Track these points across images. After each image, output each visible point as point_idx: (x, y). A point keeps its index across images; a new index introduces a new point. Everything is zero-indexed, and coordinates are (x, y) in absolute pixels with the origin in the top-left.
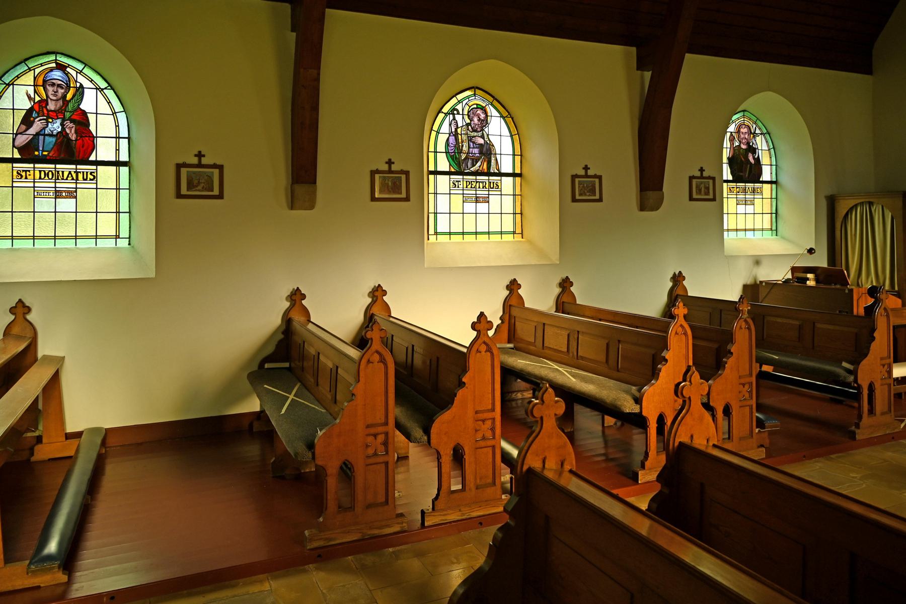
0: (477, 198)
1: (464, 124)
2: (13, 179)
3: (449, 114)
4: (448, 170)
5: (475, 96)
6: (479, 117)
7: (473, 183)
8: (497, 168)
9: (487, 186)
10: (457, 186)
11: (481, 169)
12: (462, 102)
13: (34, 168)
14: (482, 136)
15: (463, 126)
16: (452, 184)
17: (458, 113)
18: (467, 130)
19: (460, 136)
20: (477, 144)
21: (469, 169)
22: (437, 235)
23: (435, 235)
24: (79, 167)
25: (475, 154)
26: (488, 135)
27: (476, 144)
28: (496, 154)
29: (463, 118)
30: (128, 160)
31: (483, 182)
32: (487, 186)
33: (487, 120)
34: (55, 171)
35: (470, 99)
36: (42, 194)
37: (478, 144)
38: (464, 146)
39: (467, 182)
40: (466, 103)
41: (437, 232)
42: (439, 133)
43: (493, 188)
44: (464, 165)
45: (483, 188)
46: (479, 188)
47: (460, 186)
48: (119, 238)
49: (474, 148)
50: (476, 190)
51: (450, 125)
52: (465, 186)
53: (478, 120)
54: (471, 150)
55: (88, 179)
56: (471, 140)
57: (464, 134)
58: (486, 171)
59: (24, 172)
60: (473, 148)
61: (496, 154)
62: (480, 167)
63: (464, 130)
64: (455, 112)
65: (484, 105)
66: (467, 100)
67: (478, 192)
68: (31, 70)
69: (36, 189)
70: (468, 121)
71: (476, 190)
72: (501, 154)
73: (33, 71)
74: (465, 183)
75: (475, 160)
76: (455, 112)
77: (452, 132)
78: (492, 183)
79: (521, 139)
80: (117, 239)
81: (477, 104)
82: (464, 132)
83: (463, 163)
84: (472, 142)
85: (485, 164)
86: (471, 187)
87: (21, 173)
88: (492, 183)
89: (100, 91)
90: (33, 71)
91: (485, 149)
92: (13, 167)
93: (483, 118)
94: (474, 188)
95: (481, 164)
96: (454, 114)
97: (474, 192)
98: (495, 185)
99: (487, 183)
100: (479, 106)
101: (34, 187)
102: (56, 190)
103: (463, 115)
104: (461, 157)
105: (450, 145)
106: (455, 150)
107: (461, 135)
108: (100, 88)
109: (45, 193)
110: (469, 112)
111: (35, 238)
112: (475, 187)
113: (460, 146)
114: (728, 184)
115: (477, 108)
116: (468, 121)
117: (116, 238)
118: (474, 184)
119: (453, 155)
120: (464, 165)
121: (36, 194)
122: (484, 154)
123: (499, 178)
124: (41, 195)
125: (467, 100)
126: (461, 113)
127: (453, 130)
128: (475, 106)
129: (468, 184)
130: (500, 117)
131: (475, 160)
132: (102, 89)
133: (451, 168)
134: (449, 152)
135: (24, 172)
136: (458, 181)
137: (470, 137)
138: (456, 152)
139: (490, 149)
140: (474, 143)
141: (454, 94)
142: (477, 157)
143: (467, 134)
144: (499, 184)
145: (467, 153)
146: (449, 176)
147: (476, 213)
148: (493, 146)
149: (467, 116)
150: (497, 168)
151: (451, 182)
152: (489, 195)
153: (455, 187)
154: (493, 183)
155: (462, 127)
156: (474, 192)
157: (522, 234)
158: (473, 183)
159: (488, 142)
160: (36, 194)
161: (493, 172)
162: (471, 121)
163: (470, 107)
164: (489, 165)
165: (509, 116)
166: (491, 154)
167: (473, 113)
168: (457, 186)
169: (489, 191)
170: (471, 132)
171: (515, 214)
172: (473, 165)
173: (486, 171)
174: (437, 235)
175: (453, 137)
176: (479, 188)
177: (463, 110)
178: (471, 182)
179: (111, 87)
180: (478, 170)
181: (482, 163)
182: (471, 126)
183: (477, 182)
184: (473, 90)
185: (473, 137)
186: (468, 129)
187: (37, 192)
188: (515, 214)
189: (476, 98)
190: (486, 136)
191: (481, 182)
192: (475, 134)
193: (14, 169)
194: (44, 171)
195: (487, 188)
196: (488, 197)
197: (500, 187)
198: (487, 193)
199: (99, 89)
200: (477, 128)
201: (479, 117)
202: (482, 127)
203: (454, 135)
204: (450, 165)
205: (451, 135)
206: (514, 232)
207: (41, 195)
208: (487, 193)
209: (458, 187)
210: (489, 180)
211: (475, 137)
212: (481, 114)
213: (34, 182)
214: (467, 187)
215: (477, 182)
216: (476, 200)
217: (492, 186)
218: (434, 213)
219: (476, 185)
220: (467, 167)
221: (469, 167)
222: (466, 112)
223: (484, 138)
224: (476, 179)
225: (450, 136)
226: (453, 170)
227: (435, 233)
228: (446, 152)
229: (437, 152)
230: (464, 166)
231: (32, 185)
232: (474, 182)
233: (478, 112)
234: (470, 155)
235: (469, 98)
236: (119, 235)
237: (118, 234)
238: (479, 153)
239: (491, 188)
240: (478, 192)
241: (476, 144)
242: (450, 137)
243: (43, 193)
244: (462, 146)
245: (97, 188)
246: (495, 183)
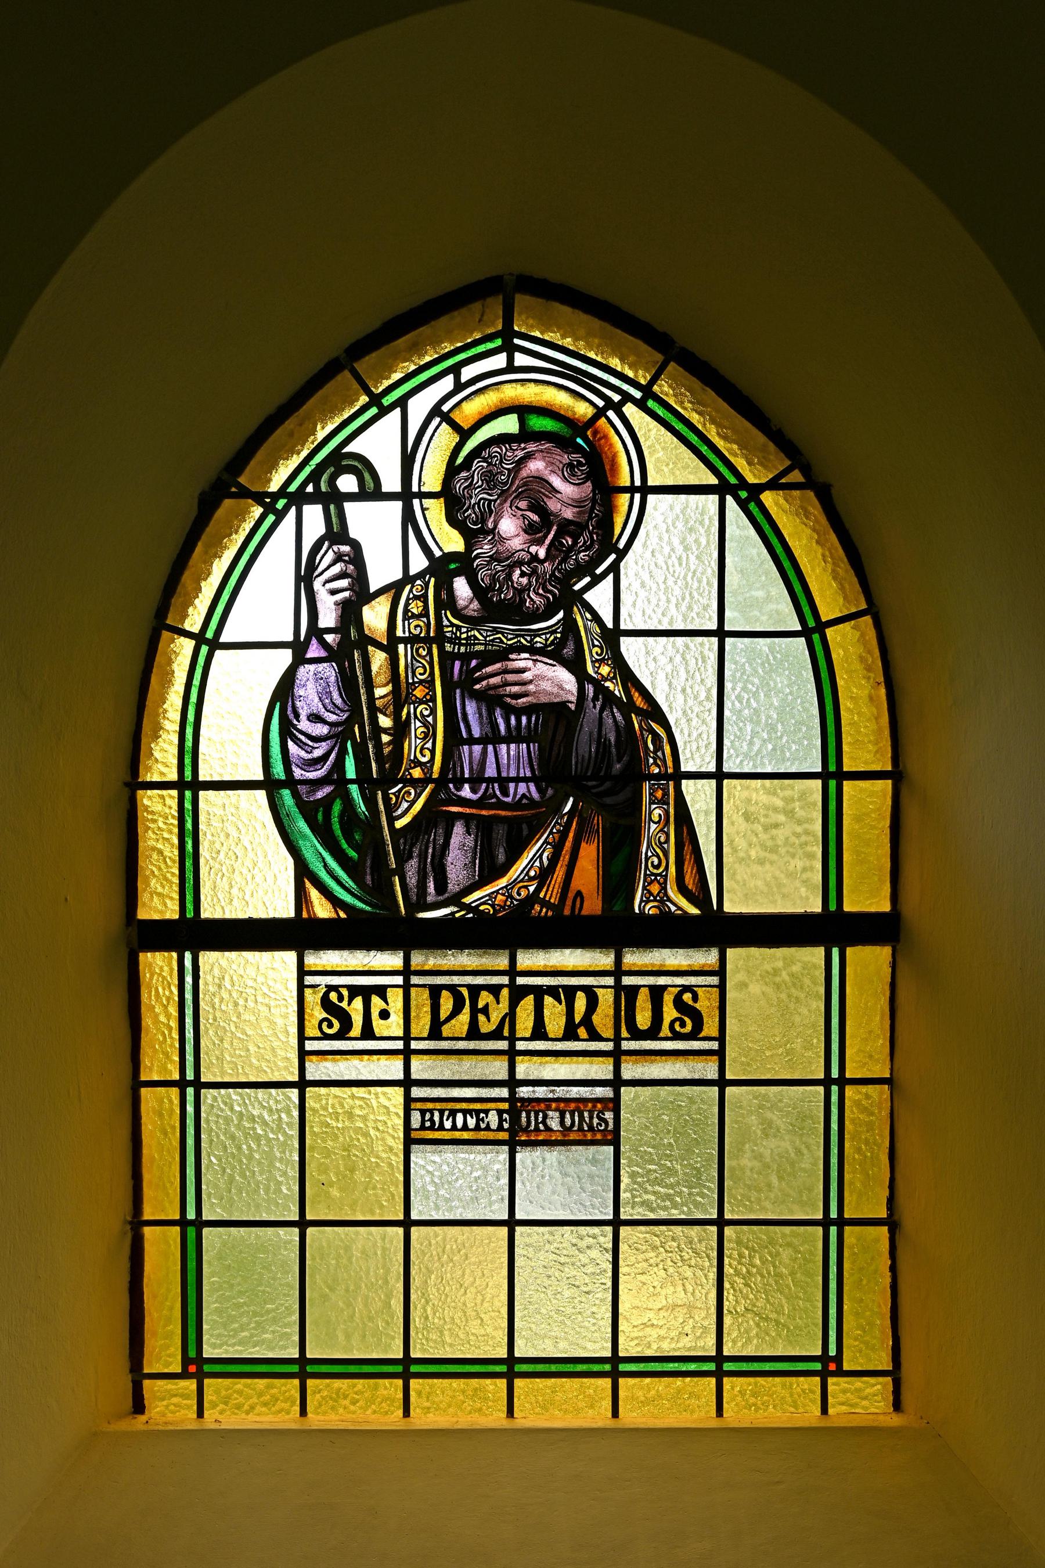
0: (515, 1106)
1: (419, 562)
2: (302, 1038)
3: (299, 499)
4: (286, 910)
5: (510, 349)
6: (538, 507)
7: (485, 998)
8: (690, 881)
9: (603, 1019)
10: (356, 1030)
11: (551, 893)
12: (402, 403)
13: (406, 972)
14: (561, 644)
15: (407, 579)
16: (316, 1013)
17: (370, 492)
18: (439, 606)
19: (378, 659)
20: (519, 712)
21: (455, 900)
22: (200, 1377)
23: (183, 1375)
24: (633, 958)
25: (503, 782)
26: (612, 637)
27: (508, 710)
28: (679, 776)
29: (408, 518)
30: (886, 907)
31: (570, 992)
32: (603, 1019)
33: (606, 523)
34: (618, 987)
35: (468, 373)
36: (448, 1124)
37: (530, 710)
38: (417, 728)
39: (435, 992)
40: (436, 411)
41: (200, 1360)
42: (216, 645)
43: (652, 1033)
44: (412, 867)
45: (570, 1033)
46: (539, 1032)
47: (379, 1026)
48: (841, 1373)
49: (492, 738)
50: (512, 1055)
51: (305, 578)
52: (422, 1025)
53: (530, 529)
54: (471, 753)
55: (665, 1031)
56: (467, 682)
57: (412, 640)
58: (593, 905)
59: (358, 1002)
60: (483, 741)
61: (679, 776)
62: (544, 875)
63: (416, 608)
64: (347, 483)
65: (583, 410)
66: (447, 384)
67: (524, 1069)
68: (384, 411)
69: (416, 1092)
70: (453, 542)
71: (512, 1055)
72: (719, 776)
73: (397, 412)
74: (421, 999)
75: (500, 832)
76: (347, 483)
77: (316, 632)
78: (643, 1001)
79: (897, 654)
80: (831, 1380)
81: (522, 410)
82: (416, 627)
83: (403, 858)
84: (478, 696)
85: (589, 854)
86: (474, 1033)
87: (344, 1004)
88: (643, 1001)
89: (743, 505)
90: (397, 412)
91: (584, 746)
92: (302, 972)
93: (568, 514)
94: (496, 1035)
95: (554, 860)
96: (334, 500)
97: (498, 1069)
98: (670, 1013)
99: (606, 998)
100: (538, 423)
101: (407, 1083)
102: (512, 1099)
103: (406, 496)
104: (390, 809)
105: (304, 725)
106: (340, 764)
107: (390, 648)
108: (743, 483)
109: (460, 1118)
110: (452, 471)
111: (623, 1367)
112: (506, 1029)
113: (377, 730)
114: (315, 960)
115: (525, 435)
116: (453, 542)
117: (824, 1375)
118: (499, 1010)
119: (327, 803)
120: (412, 867)
121: (416, 1119)
122: (577, 786)
123: (708, 958)
124: (442, 1128)
125: (447, 384)
126: (391, 482)
127: (328, 618)
128: (509, 424)
129: (444, 1014)
130: (721, 490)
131: (500, 832)
132: (756, 491)
133: (314, 894)
134: (290, 782)
135: (358, 1002)
136: (366, 993)
137: (465, 658)
138: (351, 772)
139: (628, 738)
140: (491, 700)
141: (334, 346)
142: (516, 805)
143: (440, 638)
144: (706, 1004)
145: (441, 783)
146: (291, 956)
147: (511, 1223)
148: (655, 712)
149: (436, 509)
150: (690, 881)
151: (312, 998)
152: (617, 1082)
153: (341, 1035)
154: (656, 993)
155: (395, 588)
156: (498, 1069)
157: (895, 1373)
158: (485, 998)
159: (615, 688)
160: (416, 1119)
161: (650, 909)
162: (470, 537)
163: (465, 434)
164: (618, 865)
165: (796, 476)
166: (635, 775)
167: (490, 479)
168: (356, 1030)
169: (617, 1055)
170: (474, 622)
171: (842, 1222)
172: (490, 871)
173: (593, 905)
174: (200, 1377)
175: (329, 671)
176: (539, 1032)
177: (408, 461)
178: (475, 991)
179: (806, 470)
180: (532, 899)
181: (558, 848)
182: (473, 583)
183: (518, 994)
184: (495, 306)
185: (488, 657)
186: (447, 601)
187: (423, 1112)
188: (842, 1222)
189: (521, 360)
190: (591, 653)
191: (553, 991)
192: (507, 633)
193: (309, 980)
194: (452, 989)
195: (608, 1033)
196: (615, 1104)
197: (710, 1027)
198: (603, 1069)
199: (733, 491)
200: (521, 591)
201: (538, 507)
202: (565, 581)
203: (332, 655)
204: (303, 872)
205: (314, 651)
206: (824, 1358)
207: (442, 1128)
208: (603, 1069)
209: (368, 1033)
210: (618, 972)
211: (503, 654)
212: (556, 482)
213: (407, 1053)
214: (435, 1033)
215: (518, 994)
216: (515, 1128)
217: (643, 1019)
218: (183, 1223)
219: (511, 1015)
220: (442, 886)
221: (453, 887)
222: (431, 476)
223: (575, 665)
224: (512, 972)
225: (300, 659)
226: (322, 910)
227: (186, 1361)
228: (269, 785)
229: (198, 786)
230: (412, 880)
231: (394, 1068)
232: (495, 990)
233: (536, 466)
234: (466, 792)
235: (455, 370)
236: (839, 1358)
237: (832, 1352)
238: (533, 779)
239: (637, 1034)
240: (524, 1069)
241: (508, 710)
242: (305, 672)
243: (453, 1113)
244: (401, 730)
245: (722, 1083)
246: (668, 999)
